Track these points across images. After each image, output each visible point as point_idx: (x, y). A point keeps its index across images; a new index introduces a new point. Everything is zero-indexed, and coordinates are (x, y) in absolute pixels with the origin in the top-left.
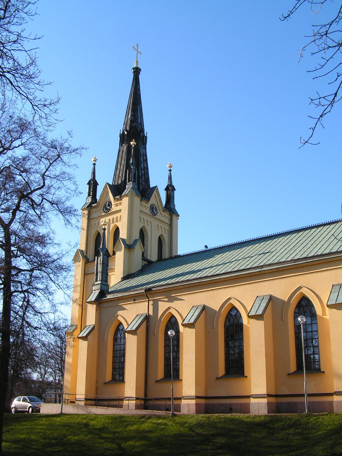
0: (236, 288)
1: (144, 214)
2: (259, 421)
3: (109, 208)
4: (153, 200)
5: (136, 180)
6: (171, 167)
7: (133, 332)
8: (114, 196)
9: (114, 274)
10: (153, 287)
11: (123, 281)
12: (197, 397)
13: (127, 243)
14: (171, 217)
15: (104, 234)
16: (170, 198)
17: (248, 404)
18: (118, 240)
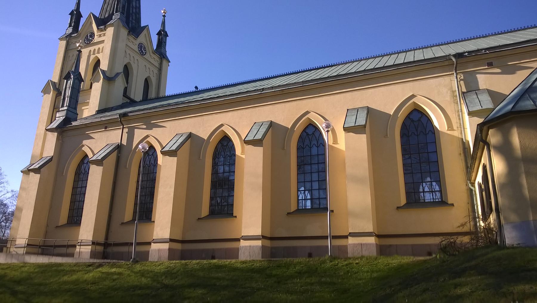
0: (230, 113)
1: (132, 51)
2: (260, 268)
3: (91, 39)
4: (142, 38)
5: (125, 12)
6: (165, 13)
7: (99, 162)
8: (98, 26)
9: (88, 108)
10: (131, 112)
11: (97, 114)
12: (171, 240)
13: (107, 75)
14: (161, 61)
15: (78, 56)
16: (162, 42)
17: (237, 250)
18: (97, 71)
